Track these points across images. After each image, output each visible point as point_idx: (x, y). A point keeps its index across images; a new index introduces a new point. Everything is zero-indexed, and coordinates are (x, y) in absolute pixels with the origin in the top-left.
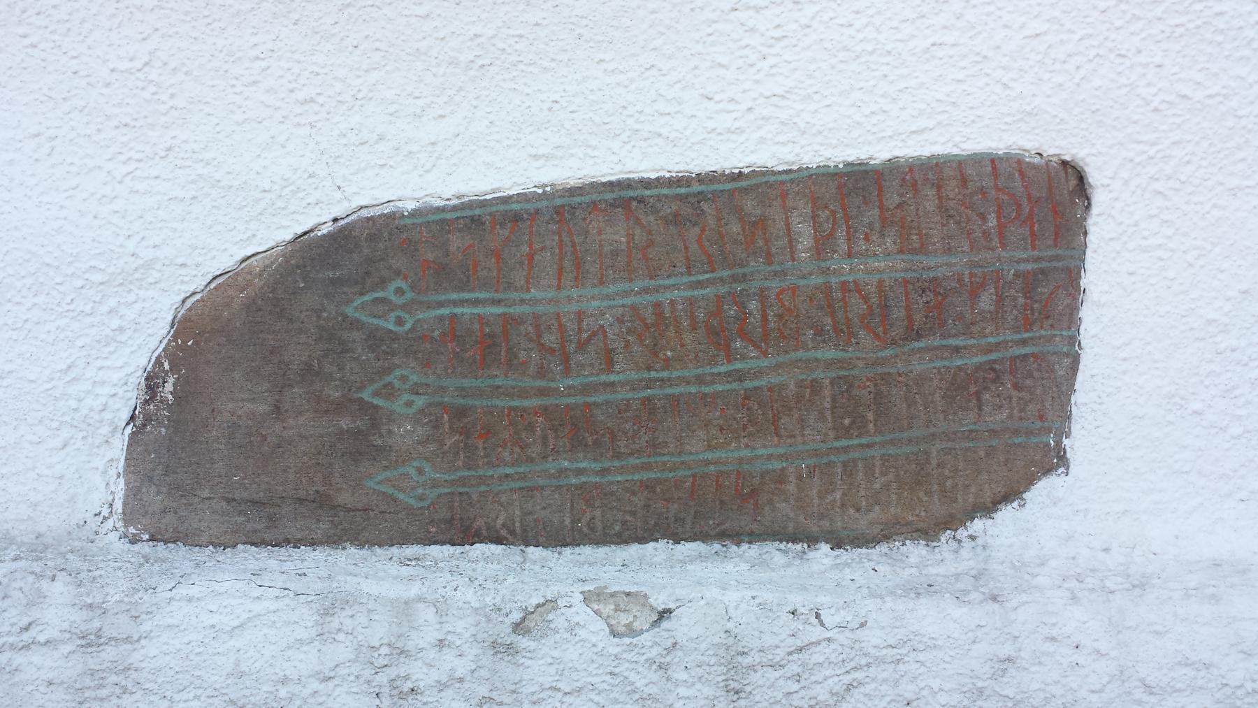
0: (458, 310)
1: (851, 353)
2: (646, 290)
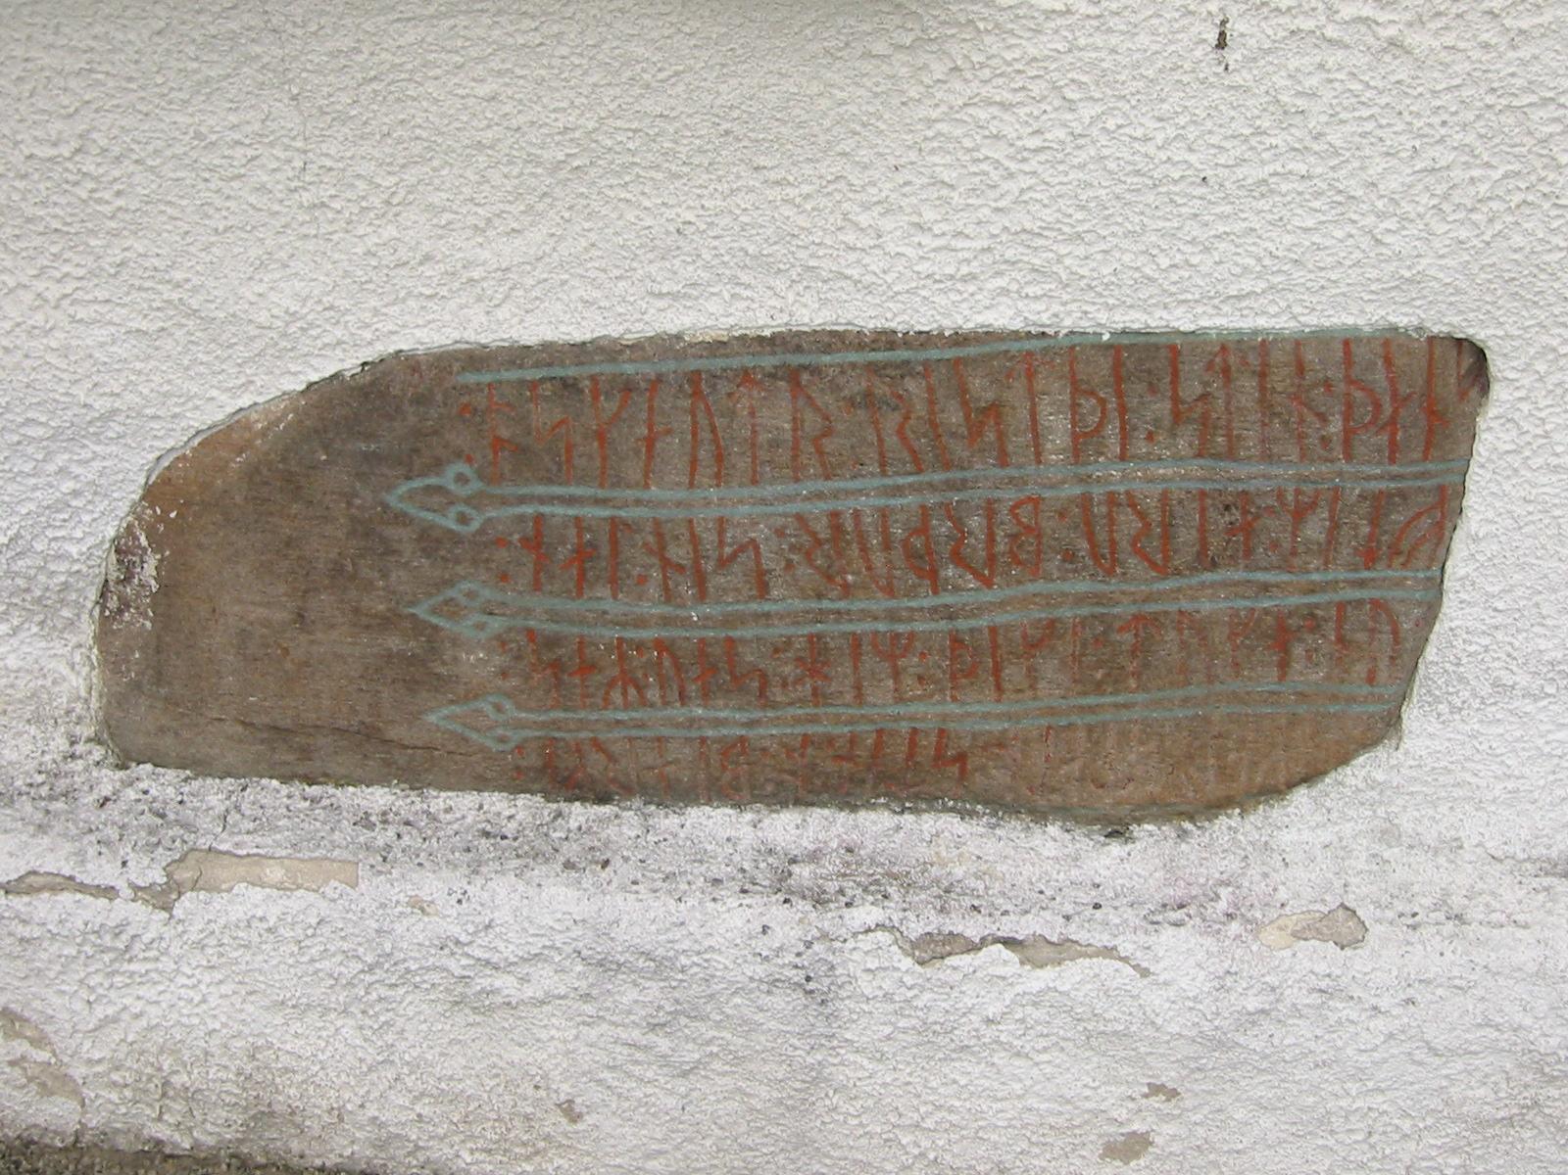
0: (546, 509)
1: (1113, 586)
2: (819, 496)
